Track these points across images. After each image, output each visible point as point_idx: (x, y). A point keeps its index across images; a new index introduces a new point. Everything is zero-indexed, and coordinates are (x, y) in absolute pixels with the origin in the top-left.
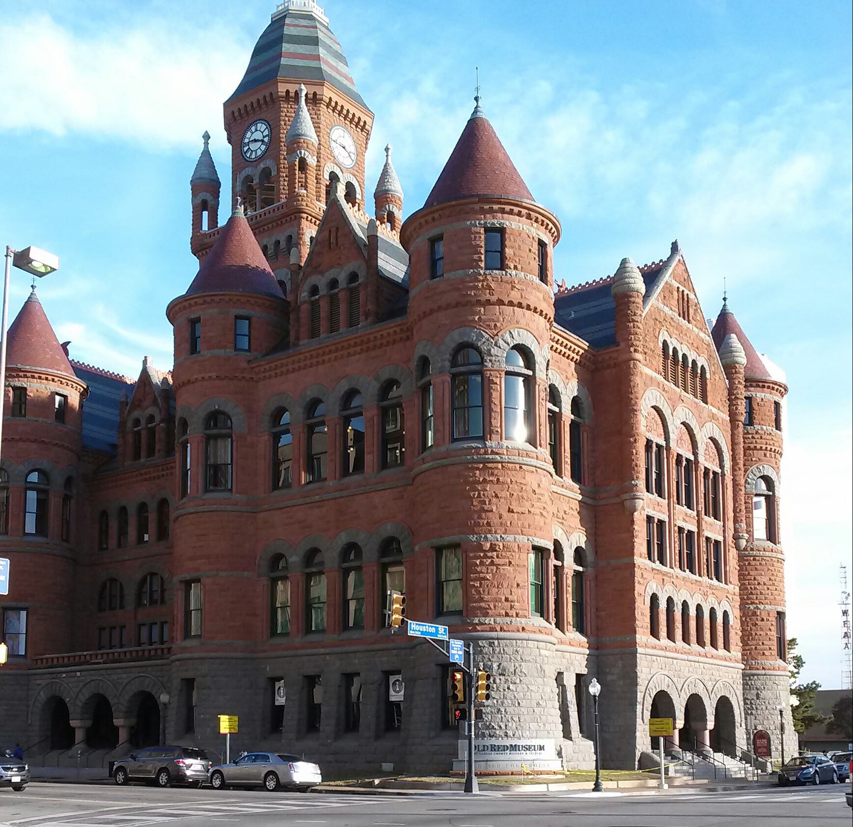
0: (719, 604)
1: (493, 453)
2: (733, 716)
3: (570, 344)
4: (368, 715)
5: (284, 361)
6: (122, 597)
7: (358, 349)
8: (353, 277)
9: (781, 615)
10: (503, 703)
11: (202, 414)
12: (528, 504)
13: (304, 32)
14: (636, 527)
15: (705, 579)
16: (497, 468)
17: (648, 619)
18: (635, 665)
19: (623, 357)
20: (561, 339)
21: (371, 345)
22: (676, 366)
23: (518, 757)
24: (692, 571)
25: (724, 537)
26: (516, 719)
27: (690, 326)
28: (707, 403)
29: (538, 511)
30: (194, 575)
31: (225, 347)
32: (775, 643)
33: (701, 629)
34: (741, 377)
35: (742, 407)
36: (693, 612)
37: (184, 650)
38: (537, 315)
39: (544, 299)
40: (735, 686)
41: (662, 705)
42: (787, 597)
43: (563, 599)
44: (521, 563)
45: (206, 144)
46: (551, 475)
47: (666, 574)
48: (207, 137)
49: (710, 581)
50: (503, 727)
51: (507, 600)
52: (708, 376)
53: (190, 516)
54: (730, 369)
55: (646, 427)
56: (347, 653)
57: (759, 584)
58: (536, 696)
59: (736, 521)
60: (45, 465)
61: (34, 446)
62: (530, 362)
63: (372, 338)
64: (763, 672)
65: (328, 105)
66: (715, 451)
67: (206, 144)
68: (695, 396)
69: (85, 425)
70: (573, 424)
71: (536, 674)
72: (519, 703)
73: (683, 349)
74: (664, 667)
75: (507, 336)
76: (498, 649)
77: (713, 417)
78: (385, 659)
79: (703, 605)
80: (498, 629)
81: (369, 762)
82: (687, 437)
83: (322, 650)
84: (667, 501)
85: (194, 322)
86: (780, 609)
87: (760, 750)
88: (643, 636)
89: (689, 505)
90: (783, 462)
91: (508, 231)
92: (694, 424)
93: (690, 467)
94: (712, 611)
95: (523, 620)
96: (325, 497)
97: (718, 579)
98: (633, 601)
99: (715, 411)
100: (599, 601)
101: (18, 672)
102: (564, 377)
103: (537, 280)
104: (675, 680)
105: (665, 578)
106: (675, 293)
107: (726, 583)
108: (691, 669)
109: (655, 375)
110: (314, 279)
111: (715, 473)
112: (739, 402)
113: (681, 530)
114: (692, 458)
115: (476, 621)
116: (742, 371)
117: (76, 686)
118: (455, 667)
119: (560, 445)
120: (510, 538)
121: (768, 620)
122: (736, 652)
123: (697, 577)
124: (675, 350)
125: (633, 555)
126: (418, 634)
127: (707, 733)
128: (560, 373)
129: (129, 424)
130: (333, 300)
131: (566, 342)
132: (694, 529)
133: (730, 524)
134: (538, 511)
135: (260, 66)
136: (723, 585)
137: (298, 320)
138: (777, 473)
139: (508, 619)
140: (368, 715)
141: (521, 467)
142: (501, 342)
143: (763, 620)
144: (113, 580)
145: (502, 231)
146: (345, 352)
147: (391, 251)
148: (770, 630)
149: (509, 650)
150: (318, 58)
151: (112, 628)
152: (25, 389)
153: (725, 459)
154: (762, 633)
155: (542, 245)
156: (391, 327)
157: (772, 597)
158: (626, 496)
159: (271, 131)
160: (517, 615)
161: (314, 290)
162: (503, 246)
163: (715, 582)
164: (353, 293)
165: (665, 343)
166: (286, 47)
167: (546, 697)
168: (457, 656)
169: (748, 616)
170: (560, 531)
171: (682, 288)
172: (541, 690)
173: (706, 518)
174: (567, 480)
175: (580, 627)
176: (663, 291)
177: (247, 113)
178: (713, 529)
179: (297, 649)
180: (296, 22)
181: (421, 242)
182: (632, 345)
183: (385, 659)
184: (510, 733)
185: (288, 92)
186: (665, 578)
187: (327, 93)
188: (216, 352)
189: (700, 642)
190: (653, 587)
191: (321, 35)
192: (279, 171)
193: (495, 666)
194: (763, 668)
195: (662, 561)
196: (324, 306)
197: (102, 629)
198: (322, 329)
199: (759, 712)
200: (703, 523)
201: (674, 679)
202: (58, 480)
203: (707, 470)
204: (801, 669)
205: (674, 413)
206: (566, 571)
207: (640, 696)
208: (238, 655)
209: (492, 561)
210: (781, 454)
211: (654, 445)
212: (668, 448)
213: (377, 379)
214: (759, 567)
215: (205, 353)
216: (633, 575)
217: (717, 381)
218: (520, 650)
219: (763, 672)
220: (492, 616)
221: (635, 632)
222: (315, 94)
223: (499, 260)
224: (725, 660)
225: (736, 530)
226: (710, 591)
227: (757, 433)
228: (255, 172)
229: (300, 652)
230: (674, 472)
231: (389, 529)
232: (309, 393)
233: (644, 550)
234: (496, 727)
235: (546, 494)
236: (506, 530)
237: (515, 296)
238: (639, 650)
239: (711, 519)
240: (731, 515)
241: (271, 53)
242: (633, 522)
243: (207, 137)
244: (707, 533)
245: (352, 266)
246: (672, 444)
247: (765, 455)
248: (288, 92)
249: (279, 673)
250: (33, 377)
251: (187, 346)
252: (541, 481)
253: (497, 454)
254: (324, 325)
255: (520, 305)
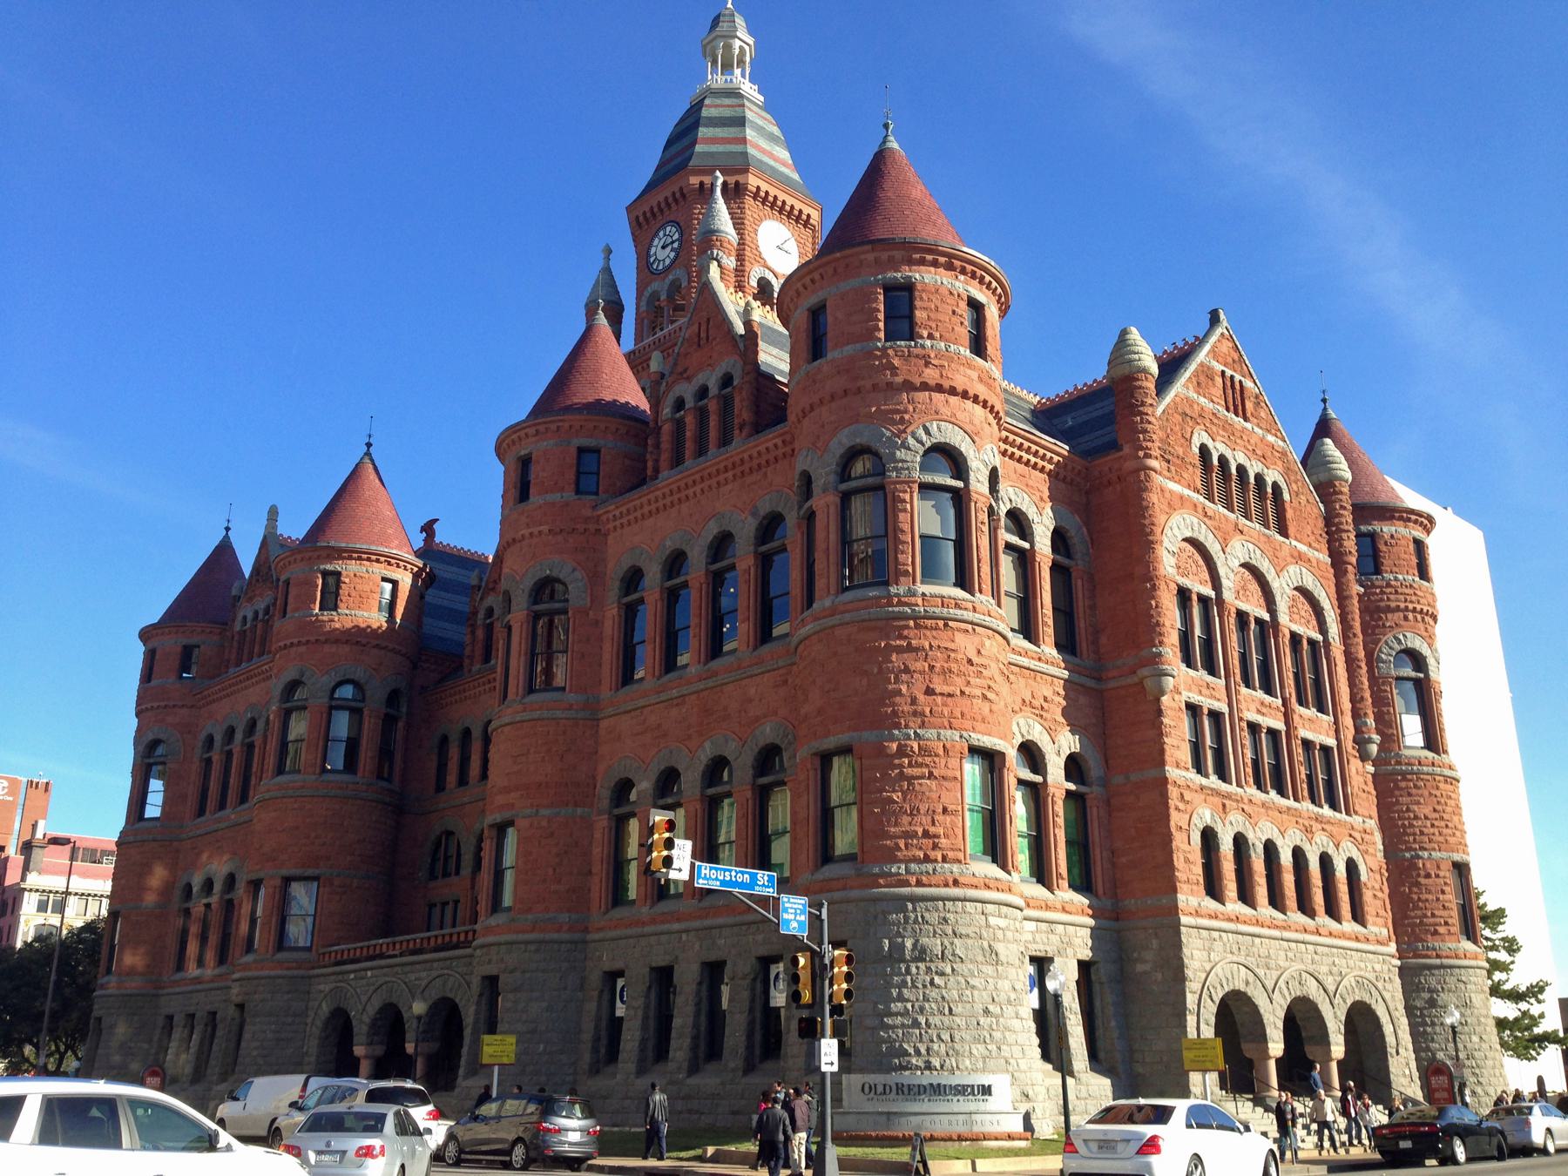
0: (1337, 846)
1: (900, 603)
2: (1383, 1036)
3: (1042, 451)
4: (735, 1035)
5: (638, 502)
6: (459, 855)
7: (730, 474)
8: (727, 380)
9: (1461, 869)
10: (922, 1009)
11: (529, 583)
12: (959, 681)
13: (727, 113)
14: (1166, 721)
15: (1307, 805)
16: (907, 627)
17: (1198, 870)
18: (1178, 945)
19: (1129, 465)
20: (1026, 444)
21: (746, 467)
22: (1221, 479)
23: (972, 1106)
24: (1282, 792)
25: (1338, 739)
26: (946, 1037)
27: (1248, 425)
28: (1287, 537)
29: (978, 692)
30: (507, 815)
31: (562, 490)
32: (1455, 913)
33: (1312, 889)
34: (1346, 500)
35: (1350, 544)
36: (1286, 858)
37: (489, 930)
38: (969, 403)
39: (980, 379)
40: (1380, 985)
41: (1236, 1014)
42: (1469, 839)
43: (1047, 835)
44: (950, 773)
45: (608, 259)
46: (1004, 637)
47: (1228, 796)
48: (608, 251)
49: (1316, 809)
50: (923, 1051)
51: (926, 834)
52: (1286, 496)
53: (506, 729)
54: (1326, 489)
55: (1171, 562)
56: (711, 928)
57: (1416, 818)
58: (981, 998)
59: (1356, 714)
60: (359, 674)
61: (347, 648)
62: (958, 464)
63: (746, 456)
64: (1438, 961)
65: (756, 196)
66: (1307, 607)
67: (608, 259)
68: (1230, 508)
69: (426, 620)
70: (1055, 567)
71: (980, 958)
72: (950, 1010)
73: (1237, 458)
74: (1227, 951)
75: (921, 433)
76: (912, 916)
77: (1299, 558)
78: (760, 937)
79: (1306, 847)
80: (913, 880)
81: (734, 1113)
82: (1254, 587)
83: (676, 926)
84: (1222, 682)
85: (525, 462)
86: (1457, 857)
87: (1437, 1095)
88: (1190, 897)
89: (1269, 690)
90: (1440, 630)
91: (919, 287)
92: (1265, 566)
93: (1267, 629)
94: (1325, 860)
95: (955, 868)
96: (685, 690)
97: (1334, 806)
98: (1167, 839)
99: (1302, 548)
100: (1110, 839)
101: (296, 972)
102: (1036, 499)
103: (966, 352)
104: (1261, 972)
105: (1227, 802)
106: (1219, 380)
107: (1348, 813)
108: (1290, 955)
109: (1187, 492)
110: (687, 390)
111: (1312, 642)
112: (1344, 536)
113: (1254, 728)
114: (1267, 617)
115: (876, 870)
116: (1346, 490)
117: (364, 990)
118: (794, 943)
119: (1035, 598)
120: (930, 733)
121: (1437, 876)
122: (1379, 926)
123: (1291, 803)
124: (1223, 461)
125: (1162, 763)
126: (715, 885)
127: (1272, 1065)
128: (1020, 488)
129: (481, 615)
130: (702, 414)
131: (1034, 448)
132: (1279, 725)
133: (1347, 720)
134: (978, 692)
135: (671, 159)
136: (1343, 816)
137: (657, 446)
138: (1430, 646)
139: (930, 867)
140: (735, 1035)
141: (946, 625)
142: (911, 441)
143: (1428, 876)
144: (450, 834)
145: (909, 288)
146: (713, 482)
147: (773, 339)
148: (1443, 892)
149: (933, 917)
150: (744, 141)
151: (445, 904)
152: (339, 574)
153: (1328, 620)
154: (1430, 897)
155: (976, 306)
156: (771, 439)
157: (1441, 839)
158: (1145, 672)
159: (681, 235)
160: (944, 859)
161: (680, 404)
162: (912, 308)
163: (1326, 811)
164: (726, 403)
165: (1204, 451)
166: (703, 132)
167: (1002, 997)
168: (795, 924)
169: (1403, 871)
170: (1038, 728)
171: (1229, 373)
172: (991, 987)
173: (1302, 710)
174: (1050, 650)
175: (1082, 884)
176: (1196, 374)
177: (654, 215)
178: (1314, 727)
179: (644, 924)
180: (718, 102)
181: (800, 316)
182: (1142, 448)
183: (760, 937)
184: (936, 1062)
185: (702, 184)
186: (1227, 802)
187: (753, 181)
188: (550, 497)
189: (1305, 907)
190: (1205, 815)
191: (749, 115)
192: (690, 281)
193: (909, 944)
194: (1438, 956)
195: (1223, 775)
196: (690, 421)
197: (432, 906)
198: (688, 453)
199: (1438, 1029)
200: (1296, 717)
201: (1257, 971)
202: (377, 696)
203: (1295, 639)
204: (1518, 956)
205: (1228, 550)
206: (1051, 790)
207: (1191, 1000)
208: (565, 936)
209: (902, 773)
210: (1435, 618)
211: (1305, 642)
212: (1220, 601)
213: (754, 514)
214: (1414, 791)
215: (535, 499)
216: (1164, 797)
217: (1304, 504)
218: (950, 916)
219: (1438, 961)
220: (901, 861)
221: (1175, 891)
222: (737, 183)
223: (902, 322)
224: (1357, 939)
225: (1358, 730)
226: (1316, 826)
227: (1389, 585)
228: (660, 287)
229: (648, 929)
230: (1234, 637)
231: (767, 733)
232: (668, 543)
233: (1185, 755)
234: (911, 1051)
235: (993, 665)
236: (923, 723)
237: (931, 375)
238: (1184, 919)
239: (1311, 712)
240: (1347, 706)
241: (686, 141)
242: (1160, 713)
243: (608, 251)
244: (1304, 733)
245: (730, 363)
246: (1228, 595)
247: (1406, 618)
248: (702, 184)
249: (618, 965)
250: (378, 561)
251: (514, 493)
252: (983, 645)
253: (906, 604)
254: (689, 446)
255: (939, 388)
